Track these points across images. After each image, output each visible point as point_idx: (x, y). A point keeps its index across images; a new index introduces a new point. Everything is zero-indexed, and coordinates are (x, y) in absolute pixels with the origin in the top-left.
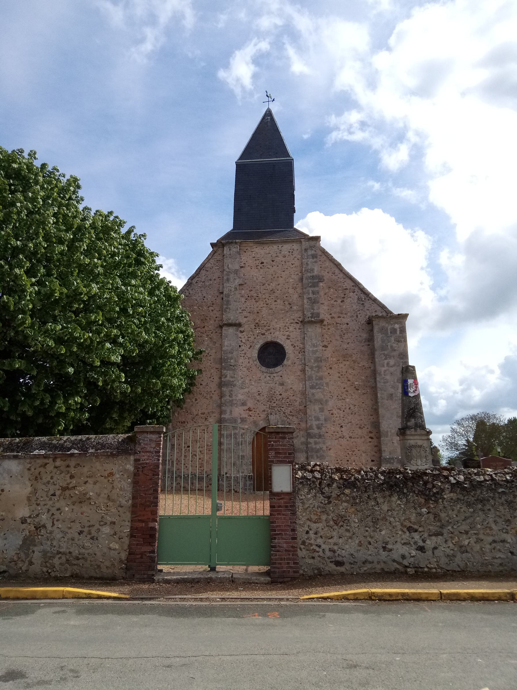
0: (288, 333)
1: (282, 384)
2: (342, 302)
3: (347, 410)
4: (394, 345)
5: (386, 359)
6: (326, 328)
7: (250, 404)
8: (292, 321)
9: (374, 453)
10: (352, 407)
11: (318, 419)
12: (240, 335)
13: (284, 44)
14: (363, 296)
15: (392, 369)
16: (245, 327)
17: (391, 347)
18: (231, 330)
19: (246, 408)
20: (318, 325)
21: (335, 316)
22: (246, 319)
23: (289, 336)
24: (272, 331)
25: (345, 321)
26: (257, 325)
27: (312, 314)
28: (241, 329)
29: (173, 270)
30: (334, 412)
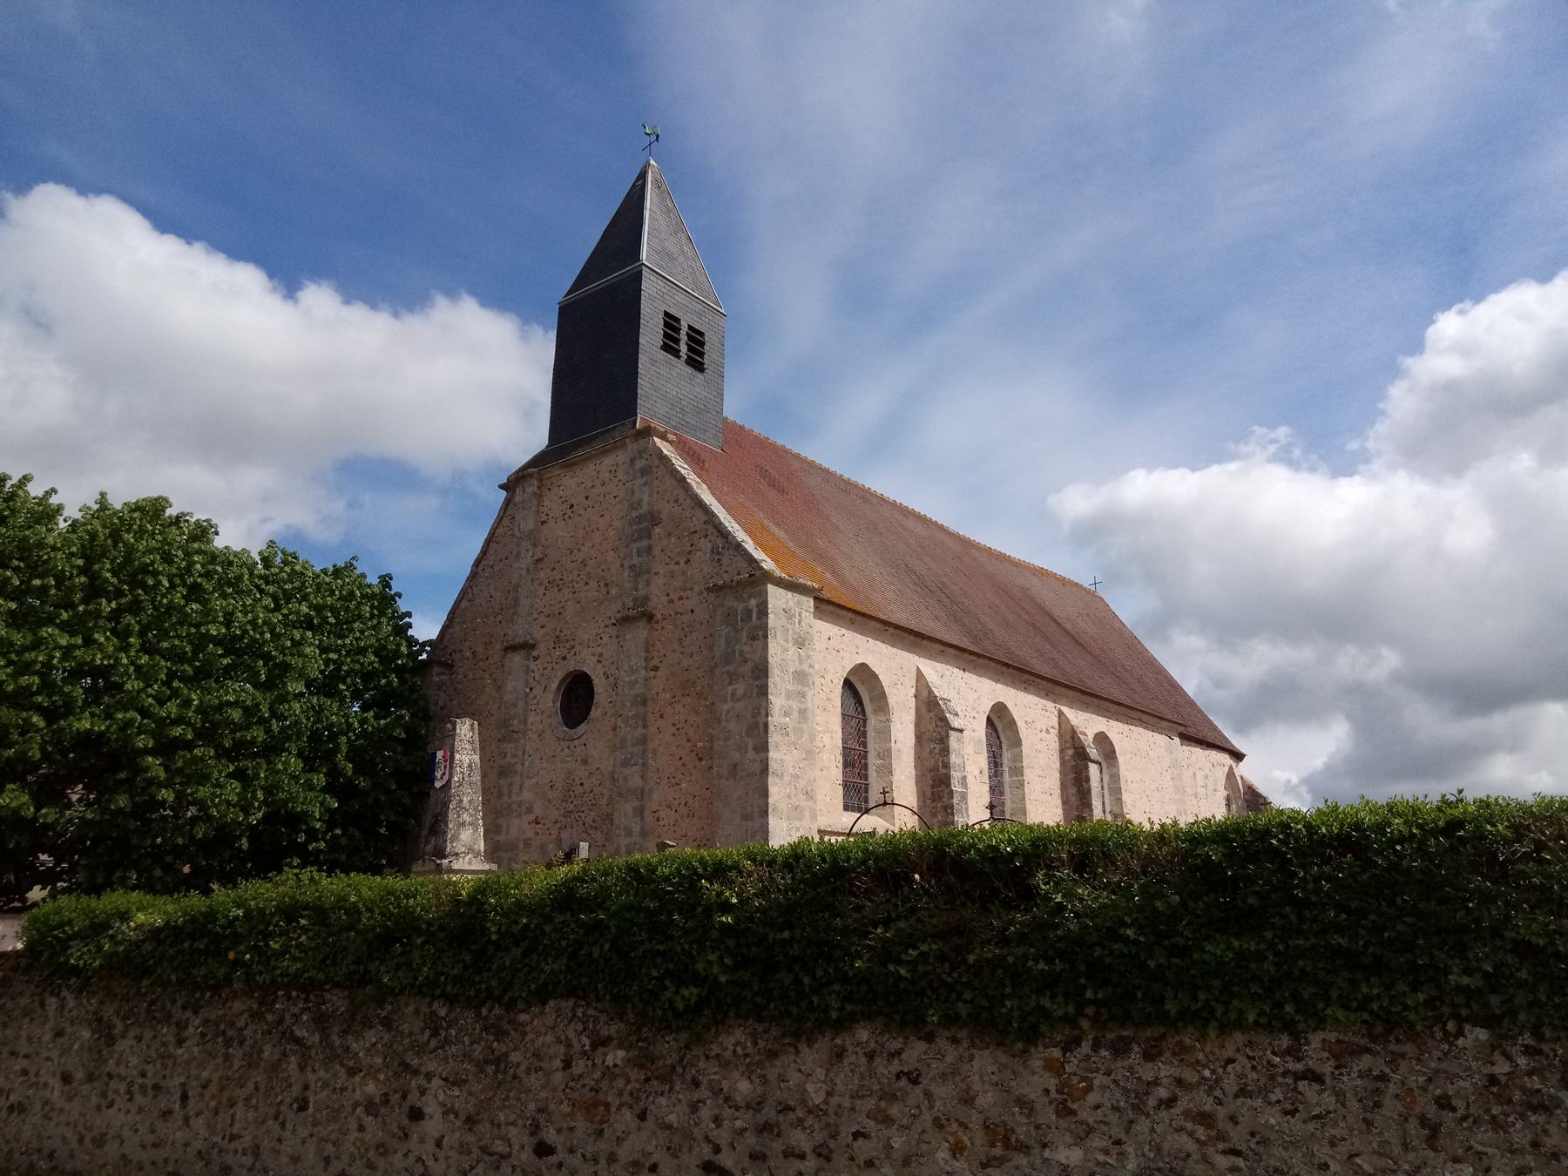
0: (599, 650)
1: (585, 762)
2: (687, 561)
3: (682, 810)
4: (747, 648)
5: (730, 683)
6: (659, 627)
7: (537, 811)
8: (608, 622)
9: (1041, 1048)
10: (690, 801)
11: (629, 833)
12: (532, 665)
13: (74, 526)
14: (720, 542)
15: (739, 706)
16: (541, 650)
17: (741, 652)
18: (517, 659)
19: (532, 817)
20: (642, 624)
21: (674, 596)
22: (542, 631)
23: (601, 655)
24: (577, 649)
25: (689, 604)
26: (558, 640)
27: (634, 600)
28: (535, 653)
29: (1297, 453)
30: (662, 814)
